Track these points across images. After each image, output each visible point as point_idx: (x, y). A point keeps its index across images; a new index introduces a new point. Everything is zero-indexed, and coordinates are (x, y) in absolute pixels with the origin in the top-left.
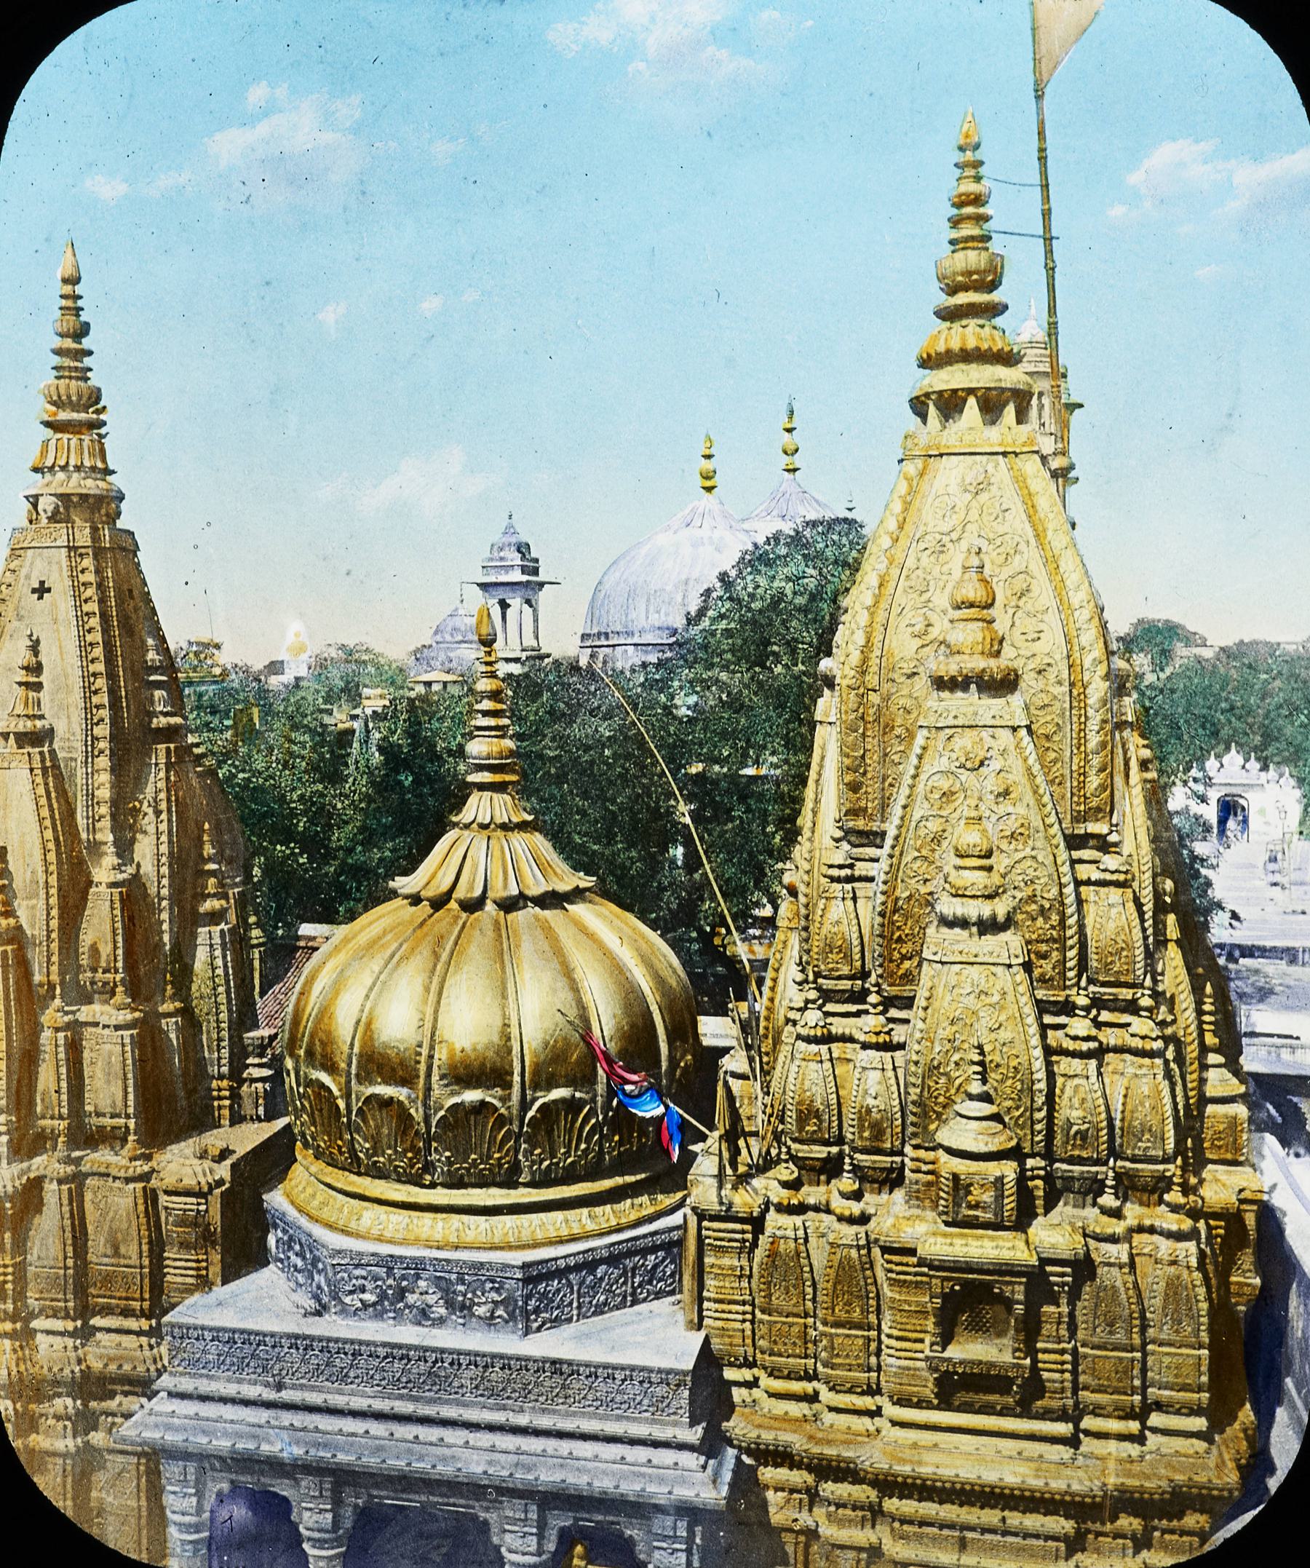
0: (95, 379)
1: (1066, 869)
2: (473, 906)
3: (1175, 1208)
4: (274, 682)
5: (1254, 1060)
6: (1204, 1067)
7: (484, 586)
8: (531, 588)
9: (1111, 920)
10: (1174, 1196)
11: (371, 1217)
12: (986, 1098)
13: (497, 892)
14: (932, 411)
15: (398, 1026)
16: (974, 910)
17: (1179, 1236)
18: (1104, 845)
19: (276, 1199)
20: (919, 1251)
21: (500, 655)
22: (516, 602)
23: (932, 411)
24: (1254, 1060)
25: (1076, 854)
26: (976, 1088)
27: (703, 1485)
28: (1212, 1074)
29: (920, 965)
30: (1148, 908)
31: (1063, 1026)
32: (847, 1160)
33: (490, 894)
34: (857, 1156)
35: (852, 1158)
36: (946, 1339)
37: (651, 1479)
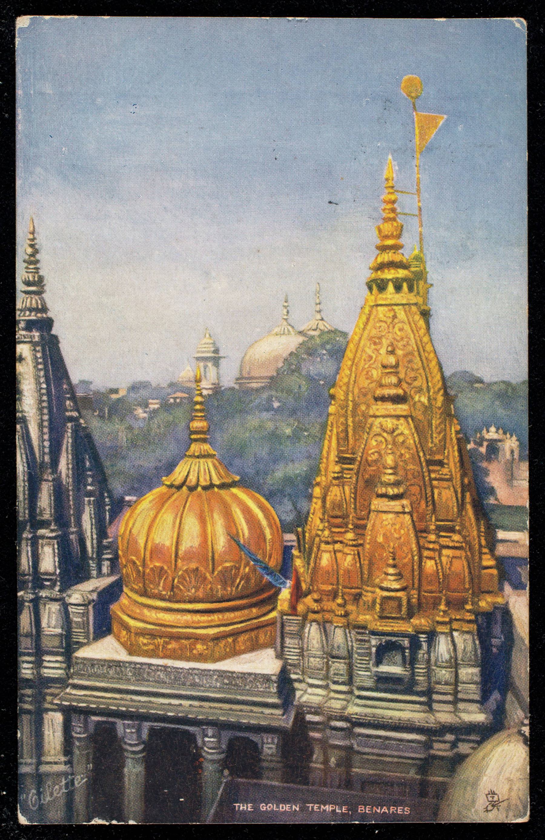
0: (41, 273)
1: (426, 474)
2: (192, 489)
3: (468, 611)
4: (114, 396)
5: (501, 550)
6: (481, 553)
7: (198, 359)
8: (216, 361)
9: (446, 496)
10: (468, 607)
11: (152, 615)
12: (394, 566)
13: (203, 483)
14: (374, 287)
15: (164, 537)
16: (391, 491)
17: (470, 622)
18: (441, 463)
19: (114, 607)
20: (369, 627)
21: (204, 386)
22: (210, 364)
23: (374, 287)
24: (501, 550)
25: (431, 468)
26: (391, 562)
27: (286, 721)
28: (484, 557)
29: (369, 513)
30: (459, 490)
31: (450, 537)
32: (340, 591)
33: (187, 483)
34: (344, 590)
35: (342, 590)
36: (378, 662)
37: (253, 717)
